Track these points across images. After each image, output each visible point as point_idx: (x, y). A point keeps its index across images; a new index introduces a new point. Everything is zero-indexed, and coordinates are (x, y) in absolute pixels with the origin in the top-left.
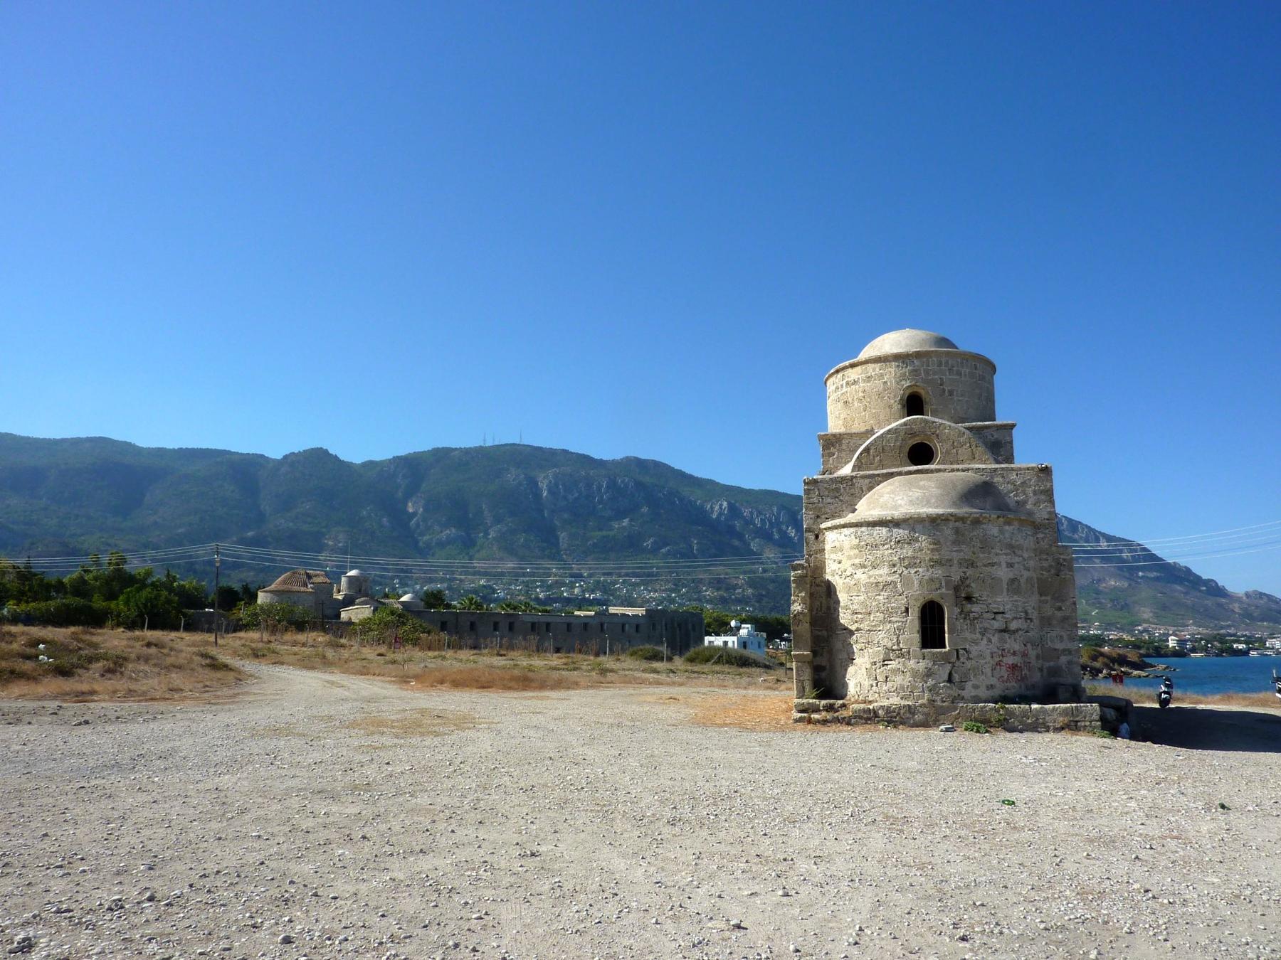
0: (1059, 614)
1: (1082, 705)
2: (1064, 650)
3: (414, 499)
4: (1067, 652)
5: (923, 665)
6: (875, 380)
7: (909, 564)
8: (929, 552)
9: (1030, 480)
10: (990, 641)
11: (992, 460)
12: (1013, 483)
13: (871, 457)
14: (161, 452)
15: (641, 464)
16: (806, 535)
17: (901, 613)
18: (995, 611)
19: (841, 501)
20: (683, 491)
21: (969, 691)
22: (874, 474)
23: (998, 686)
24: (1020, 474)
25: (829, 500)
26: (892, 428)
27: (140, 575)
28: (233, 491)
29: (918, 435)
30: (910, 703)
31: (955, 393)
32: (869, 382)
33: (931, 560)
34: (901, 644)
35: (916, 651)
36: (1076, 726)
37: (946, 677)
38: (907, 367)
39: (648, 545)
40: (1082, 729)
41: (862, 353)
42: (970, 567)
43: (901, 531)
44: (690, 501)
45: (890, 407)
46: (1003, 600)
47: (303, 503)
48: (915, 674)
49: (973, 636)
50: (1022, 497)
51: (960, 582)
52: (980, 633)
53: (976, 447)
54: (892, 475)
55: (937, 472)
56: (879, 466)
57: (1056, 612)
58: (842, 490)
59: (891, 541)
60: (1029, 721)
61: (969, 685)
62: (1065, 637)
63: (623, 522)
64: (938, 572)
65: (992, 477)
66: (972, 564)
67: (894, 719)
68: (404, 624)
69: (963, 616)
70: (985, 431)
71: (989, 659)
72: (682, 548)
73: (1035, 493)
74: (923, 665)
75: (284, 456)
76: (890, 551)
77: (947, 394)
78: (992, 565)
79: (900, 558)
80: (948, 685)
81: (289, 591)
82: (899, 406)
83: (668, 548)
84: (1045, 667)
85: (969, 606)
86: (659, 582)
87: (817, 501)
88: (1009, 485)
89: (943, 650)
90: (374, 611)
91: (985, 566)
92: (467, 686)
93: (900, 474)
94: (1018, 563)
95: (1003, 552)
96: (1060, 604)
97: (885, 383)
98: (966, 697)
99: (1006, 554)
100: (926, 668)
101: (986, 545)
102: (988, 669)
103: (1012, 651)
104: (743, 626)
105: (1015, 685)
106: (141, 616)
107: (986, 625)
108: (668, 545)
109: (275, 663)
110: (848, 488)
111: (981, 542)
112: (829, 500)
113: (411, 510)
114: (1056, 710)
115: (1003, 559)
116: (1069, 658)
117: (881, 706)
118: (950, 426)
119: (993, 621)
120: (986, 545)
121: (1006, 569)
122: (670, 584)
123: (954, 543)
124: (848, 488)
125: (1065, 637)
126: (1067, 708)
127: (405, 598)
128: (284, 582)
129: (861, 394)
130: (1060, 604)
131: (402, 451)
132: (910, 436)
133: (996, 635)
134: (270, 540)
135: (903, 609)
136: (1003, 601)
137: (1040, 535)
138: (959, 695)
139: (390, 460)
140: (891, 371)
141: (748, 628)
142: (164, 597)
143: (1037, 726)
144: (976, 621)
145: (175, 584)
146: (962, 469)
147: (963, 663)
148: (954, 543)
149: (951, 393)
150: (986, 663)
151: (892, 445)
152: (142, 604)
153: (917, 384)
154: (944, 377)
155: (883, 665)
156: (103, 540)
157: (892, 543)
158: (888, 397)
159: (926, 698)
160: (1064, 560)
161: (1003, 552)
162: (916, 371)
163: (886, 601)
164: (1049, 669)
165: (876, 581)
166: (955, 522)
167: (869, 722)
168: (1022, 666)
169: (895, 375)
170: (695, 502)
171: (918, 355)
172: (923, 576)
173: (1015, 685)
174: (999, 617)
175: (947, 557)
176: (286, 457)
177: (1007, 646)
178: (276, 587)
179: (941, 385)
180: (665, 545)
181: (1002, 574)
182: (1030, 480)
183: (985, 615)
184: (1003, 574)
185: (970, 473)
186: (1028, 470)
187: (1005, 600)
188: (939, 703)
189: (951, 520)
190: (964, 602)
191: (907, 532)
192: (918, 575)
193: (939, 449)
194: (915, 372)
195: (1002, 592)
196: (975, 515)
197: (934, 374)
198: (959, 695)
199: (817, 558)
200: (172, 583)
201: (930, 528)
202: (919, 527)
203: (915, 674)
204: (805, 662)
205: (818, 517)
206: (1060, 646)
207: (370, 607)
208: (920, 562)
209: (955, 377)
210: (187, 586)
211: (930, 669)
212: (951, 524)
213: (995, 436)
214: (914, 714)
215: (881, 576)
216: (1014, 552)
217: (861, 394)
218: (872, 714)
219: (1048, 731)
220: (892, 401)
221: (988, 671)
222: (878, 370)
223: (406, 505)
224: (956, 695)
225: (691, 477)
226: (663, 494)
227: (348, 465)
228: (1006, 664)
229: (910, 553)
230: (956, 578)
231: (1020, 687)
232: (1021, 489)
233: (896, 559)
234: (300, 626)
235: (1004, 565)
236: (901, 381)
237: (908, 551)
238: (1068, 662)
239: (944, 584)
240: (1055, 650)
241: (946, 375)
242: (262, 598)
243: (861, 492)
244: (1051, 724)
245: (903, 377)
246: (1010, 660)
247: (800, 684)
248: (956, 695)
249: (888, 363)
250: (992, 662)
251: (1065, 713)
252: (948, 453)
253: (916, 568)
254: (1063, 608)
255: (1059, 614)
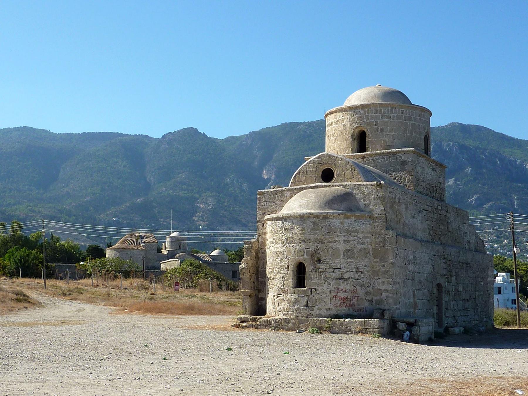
0: (383, 269)
1: (369, 319)
2: (385, 290)
3: (268, 167)
4: (386, 291)
5: (294, 296)
6: (340, 123)
7: (290, 242)
8: (299, 235)
9: (372, 191)
10: (329, 284)
11: (363, 179)
12: (363, 193)
13: (301, 178)
14: (69, 136)
15: (464, 129)
16: (258, 224)
17: (286, 269)
18: (334, 267)
19: (276, 204)
20: (504, 152)
21: (316, 312)
22: (293, 189)
23: (333, 309)
24: (368, 188)
25: (270, 204)
26: (312, 160)
27: (33, 238)
28: (125, 166)
29: (325, 164)
30: (287, 317)
31: (385, 130)
32: (337, 124)
33: (300, 239)
34: (285, 286)
35: (291, 289)
36: (366, 331)
37: (305, 303)
38: (356, 115)
39: (472, 202)
40: (368, 333)
41: (345, 103)
42: (320, 243)
43: (287, 223)
44: (510, 161)
45: (346, 140)
46: (340, 262)
47: (179, 173)
48: (290, 301)
49: (320, 281)
50: (368, 202)
51: (314, 252)
52: (324, 280)
53: (355, 171)
54: (302, 189)
55: (325, 187)
56: (304, 182)
57: (381, 268)
58: (277, 198)
59: (283, 229)
60: (343, 328)
61: (316, 308)
62: (386, 283)
63: (449, 181)
64: (303, 246)
65: (353, 190)
66: (322, 241)
67: (279, 326)
68: (199, 272)
69: (315, 270)
70: (398, 154)
71: (328, 294)
72: (503, 203)
73: (374, 199)
74: (294, 296)
75: (163, 136)
76: (282, 234)
77: (379, 131)
78: (334, 242)
79: (286, 238)
80: (305, 308)
81: (127, 249)
82: (351, 140)
83: (491, 203)
84: (374, 299)
85: (319, 265)
86: (482, 234)
87: (263, 205)
88: (361, 195)
89: (304, 289)
90: (181, 263)
91: (329, 242)
92: (150, 312)
93: (306, 188)
94: (352, 240)
95: (342, 234)
96: (384, 263)
97: (344, 125)
98: (314, 315)
99: (344, 236)
100: (295, 299)
101: (331, 230)
102: (328, 300)
103: (344, 290)
104: (499, 274)
105: (345, 308)
106: (17, 269)
107: (328, 275)
108: (490, 201)
109: (72, 299)
110: (279, 197)
111: (328, 229)
112: (270, 204)
113: (265, 177)
114: (357, 322)
115: (342, 238)
116: (387, 294)
117: (273, 319)
118: (341, 158)
119: (333, 273)
120: (331, 230)
121: (343, 244)
122: (493, 236)
123: (312, 230)
124: (279, 197)
125: (386, 283)
126: (361, 321)
127: (215, 253)
128: (124, 242)
129: (334, 132)
130: (384, 263)
131: (257, 128)
132: (321, 164)
133: (334, 281)
134: (154, 204)
135: (286, 266)
136: (340, 262)
137: (376, 224)
138: (310, 313)
139: (247, 135)
140: (348, 117)
141: (503, 276)
142: (33, 254)
143: (346, 331)
144: (322, 273)
145: (58, 244)
146: (338, 185)
147: (314, 296)
148: (312, 230)
149: (382, 130)
150: (326, 296)
151: (311, 170)
152: (18, 259)
153: (361, 125)
154: (378, 120)
155: (278, 297)
156: (30, 208)
157: (283, 230)
158: (345, 134)
159: (294, 315)
160: (387, 238)
161: (342, 234)
162: (361, 117)
163: (279, 262)
164: (376, 300)
165: (276, 251)
166: (313, 218)
167: (267, 327)
168: (352, 298)
169: (350, 120)
170: (515, 161)
171: (362, 107)
172: (296, 248)
173: (345, 308)
174: (336, 271)
175: (308, 238)
176: (164, 136)
177: (341, 287)
178: (118, 246)
179: (376, 126)
180: (489, 201)
181: (340, 247)
182: (372, 191)
183: (327, 270)
184: (342, 247)
185: (342, 188)
186: (372, 185)
187: (341, 261)
188: (300, 318)
189: (311, 217)
190: (316, 263)
191: (290, 224)
192: (294, 247)
193: (336, 171)
194: (361, 118)
195: (340, 257)
196: (324, 214)
197: (372, 118)
198: (310, 313)
199: (263, 237)
200: (55, 243)
201: (300, 221)
202: (295, 221)
203: (290, 301)
204: (247, 295)
205: (264, 213)
206: (383, 288)
207: (179, 260)
208: (295, 241)
209: (386, 120)
210: (66, 245)
211: (297, 299)
212: (311, 219)
213: (403, 158)
214: (288, 323)
215: (278, 248)
216: (350, 234)
217: (334, 132)
218: (268, 323)
219: (352, 334)
220: (348, 137)
221: (328, 301)
222: (341, 116)
223: (261, 173)
224: (309, 313)
225: (512, 139)
226: (486, 156)
227: (214, 141)
228: (339, 297)
229: (290, 236)
230: (312, 249)
231: (349, 310)
232: (367, 197)
233: (284, 239)
234: (127, 275)
235: (342, 242)
236: (352, 123)
237: (290, 235)
238: (386, 297)
239: (305, 253)
240: (380, 289)
241: (379, 119)
242: (109, 254)
243: (286, 199)
244: (353, 330)
245: (353, 122)
246: (343, 295)
247: (244, 307)
248: (309, 313)
249: (346, 112)
250: (330, 296)
251: (360, 324)
252: (340, 174)
253: (293, 244)
254: (385, 266)
255: (383, 269)
